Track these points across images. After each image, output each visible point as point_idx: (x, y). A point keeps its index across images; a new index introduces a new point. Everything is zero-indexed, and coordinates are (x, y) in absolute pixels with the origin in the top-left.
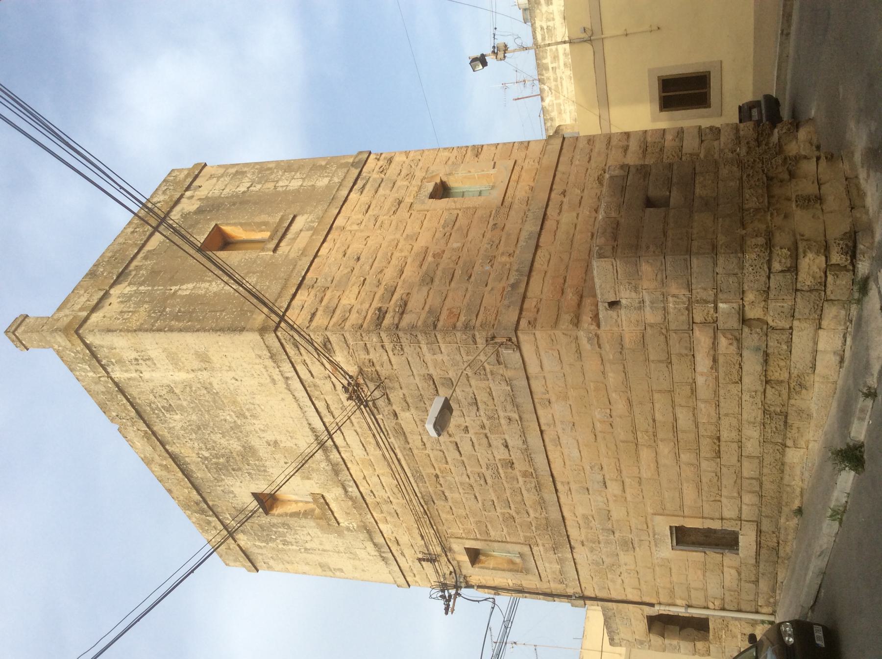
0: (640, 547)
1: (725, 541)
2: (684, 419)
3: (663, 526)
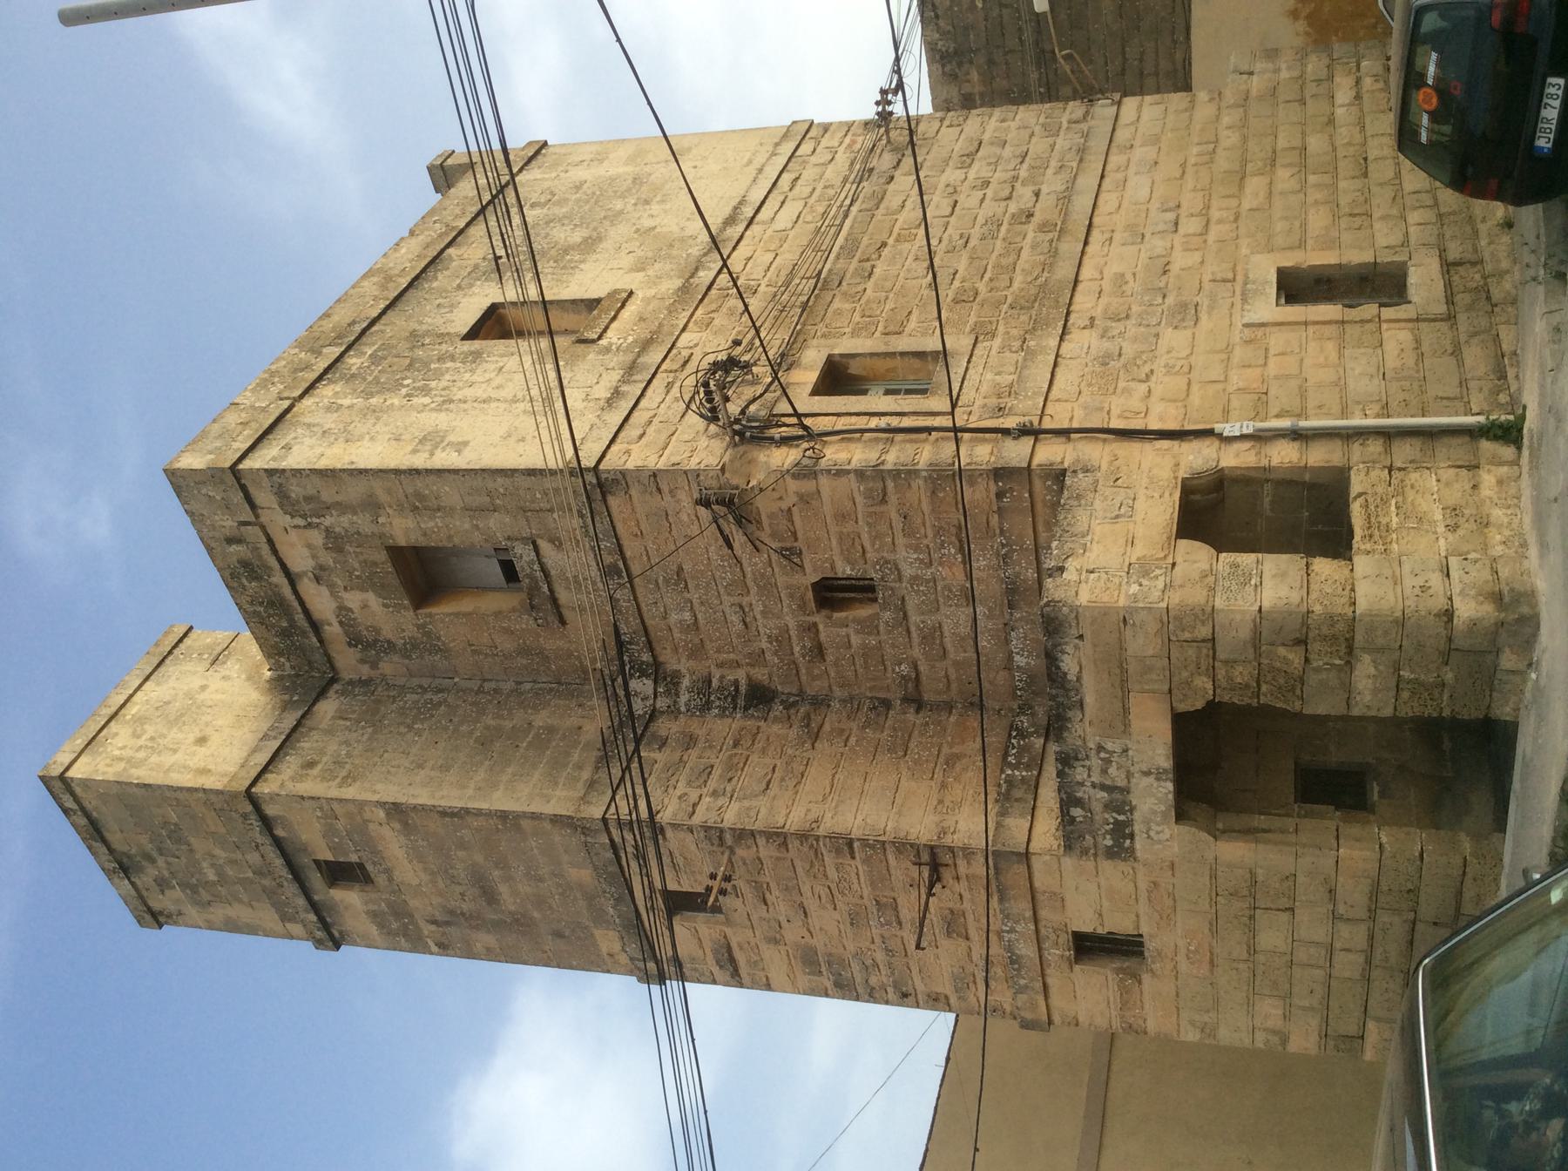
0: (1211, 308)
1: (1378, 284)
2: (1316, 143)
3: (1265, 270)
